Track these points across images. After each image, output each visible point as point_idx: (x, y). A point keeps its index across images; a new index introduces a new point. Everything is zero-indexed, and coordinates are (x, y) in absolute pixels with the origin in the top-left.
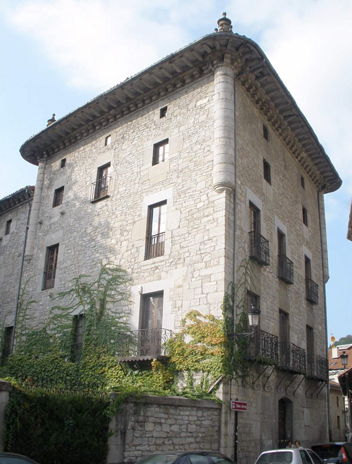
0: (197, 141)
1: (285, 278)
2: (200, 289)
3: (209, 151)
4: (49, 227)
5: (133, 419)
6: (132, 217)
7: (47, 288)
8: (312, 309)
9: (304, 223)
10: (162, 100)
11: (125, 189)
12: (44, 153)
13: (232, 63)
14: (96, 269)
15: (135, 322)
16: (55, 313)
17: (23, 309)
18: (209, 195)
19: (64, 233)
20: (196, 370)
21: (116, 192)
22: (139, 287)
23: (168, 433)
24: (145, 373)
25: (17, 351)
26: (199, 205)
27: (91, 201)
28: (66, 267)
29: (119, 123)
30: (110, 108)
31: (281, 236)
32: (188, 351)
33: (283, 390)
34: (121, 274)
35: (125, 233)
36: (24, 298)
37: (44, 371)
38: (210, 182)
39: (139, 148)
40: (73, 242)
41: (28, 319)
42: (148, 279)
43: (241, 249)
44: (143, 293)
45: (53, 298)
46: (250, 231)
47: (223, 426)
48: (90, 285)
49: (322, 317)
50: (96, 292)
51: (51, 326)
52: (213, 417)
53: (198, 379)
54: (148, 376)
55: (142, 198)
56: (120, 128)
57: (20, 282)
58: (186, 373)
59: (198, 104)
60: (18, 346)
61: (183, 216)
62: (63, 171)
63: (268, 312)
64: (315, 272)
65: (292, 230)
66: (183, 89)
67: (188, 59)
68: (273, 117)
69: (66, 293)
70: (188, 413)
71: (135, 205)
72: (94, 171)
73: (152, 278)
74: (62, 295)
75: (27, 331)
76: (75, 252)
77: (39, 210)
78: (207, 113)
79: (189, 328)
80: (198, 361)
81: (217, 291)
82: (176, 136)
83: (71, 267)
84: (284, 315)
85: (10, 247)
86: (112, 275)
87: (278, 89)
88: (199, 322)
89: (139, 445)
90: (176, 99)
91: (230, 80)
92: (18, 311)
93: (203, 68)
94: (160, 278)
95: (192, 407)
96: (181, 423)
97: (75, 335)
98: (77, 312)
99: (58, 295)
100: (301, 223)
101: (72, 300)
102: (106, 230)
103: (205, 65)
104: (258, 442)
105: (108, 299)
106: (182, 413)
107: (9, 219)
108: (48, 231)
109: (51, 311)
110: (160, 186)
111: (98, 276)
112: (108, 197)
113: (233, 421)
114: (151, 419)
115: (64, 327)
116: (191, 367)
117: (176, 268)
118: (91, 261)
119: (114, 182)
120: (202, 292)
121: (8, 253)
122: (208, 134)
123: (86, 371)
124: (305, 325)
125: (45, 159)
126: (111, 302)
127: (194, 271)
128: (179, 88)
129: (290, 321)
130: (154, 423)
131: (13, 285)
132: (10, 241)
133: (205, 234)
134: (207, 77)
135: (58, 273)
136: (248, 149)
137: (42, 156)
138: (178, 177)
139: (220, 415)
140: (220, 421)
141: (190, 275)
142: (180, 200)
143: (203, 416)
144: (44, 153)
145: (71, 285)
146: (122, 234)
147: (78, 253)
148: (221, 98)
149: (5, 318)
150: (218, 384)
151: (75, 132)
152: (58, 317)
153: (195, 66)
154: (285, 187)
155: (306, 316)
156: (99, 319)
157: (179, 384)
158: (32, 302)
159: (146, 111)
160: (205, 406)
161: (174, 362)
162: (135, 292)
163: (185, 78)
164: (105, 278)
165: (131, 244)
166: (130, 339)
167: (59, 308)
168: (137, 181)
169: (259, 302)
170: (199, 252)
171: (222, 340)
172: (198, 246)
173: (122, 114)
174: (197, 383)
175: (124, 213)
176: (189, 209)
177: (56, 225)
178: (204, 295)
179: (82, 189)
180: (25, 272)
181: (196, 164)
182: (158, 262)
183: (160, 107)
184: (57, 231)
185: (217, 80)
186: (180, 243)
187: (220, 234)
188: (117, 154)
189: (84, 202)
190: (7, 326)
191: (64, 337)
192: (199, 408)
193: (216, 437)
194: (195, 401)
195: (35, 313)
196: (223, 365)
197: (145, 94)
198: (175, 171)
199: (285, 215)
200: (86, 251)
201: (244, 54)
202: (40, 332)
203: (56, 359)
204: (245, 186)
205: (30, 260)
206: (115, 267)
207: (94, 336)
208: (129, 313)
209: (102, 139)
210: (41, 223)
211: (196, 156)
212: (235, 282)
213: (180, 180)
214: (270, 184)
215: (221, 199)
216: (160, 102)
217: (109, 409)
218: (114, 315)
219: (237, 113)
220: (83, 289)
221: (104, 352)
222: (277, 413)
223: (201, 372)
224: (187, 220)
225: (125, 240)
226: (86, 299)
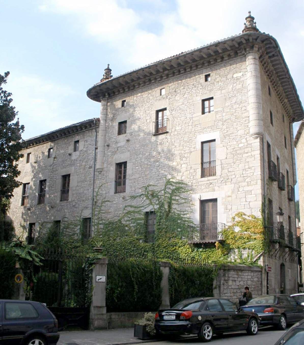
0: (236, 102)
2: (244, 199)
3: (245, 110)
4: (116, 149)
5: (223, 279)
6: (188, 149)
7: (117, 192)
10: (205, 69)
11: (180, 128)
12: (106, 94)
13: (258, 50)
14: (162, 181)
15: (197, 217)
16: (128, 210)
17: (98, 206)
18: (247, 139)
19: (130, 154)
20: (244, 248)
21: (173, 130)
22: (199, 195)
23: (238, 286)
24: (208, 250)
25: (96, 235)
26: (241, 145)
27: (153, 134)
28: (135, 179)
29: (171, 80)
30: (165, 69)
32: (238, 237)
34: (182, 186)
35: (184, 159)
36: (98, 198)
37: (124, 249)
38: (247, 131)
39: (190, 101)
40: (139, 161)
41: (104, 213)
42: (205, 190)
44: (201, 199)
45: (126, 199)
46: (165, 112)
47: (263, 280)
48: (157, 192)
50: (163, 197)
51: (126, 219)
53: (245, 254)
54: (210, 252)
55: (195, 136)
56: (172, 84)
57: (94, 186)
58: (236, 250)
59: (235, 76)
60: (96, 231)
61: (229, 151)
62: (124, 110)
66: (222, 63)
67: (228, 45)
68: (274, 80)
69: (137, 196)
70: (247, 274)
72: (153, 112)
73: (208, 190)
74: (133, 197)
75: (103, 221)
76: (142, 169)
77: (105, 136)
78: (242, 83)
79: (238, 223)
80: (245, 243)
81: (256, 201)
82: (219, 96)
83: (140, 179)
85: (80, 160)
86: (176, 186)
87: (281, 64)
88: (245, 219)
89: (226, 293)
90: (217, 70)
91: (258, 62)
92: (94, 208)
93: (238, 52)
94: (214, 190)
95: (249, 270)
97: (146, 225)
98: (148, 210)
99: (130, 198)
101: (143, 202)
102: (170, 155)
103: (240, 50)
105: (173, 202)
106: (244, 274)
107: (76, 140)
108: (116, 152)
109: (124, 208)
110: (209, 130)
111: (164, 186)
112: (167, 132)
113: (266, 278)
114: (231, 279)
115: (136, 219)
116: (241, 246)
117: (226, 185)
118: (157, 176)
119: (171, 122)
120: (246, 200)
121: (78, 165)
122: (244, 98)
123: (160, 249)
125: (106, 99)
126: (176, 204)
127: (239, 187)
128: (218, 62)
131: (86, 189)
132: (80, 156)
134: (240, 58)
137: (104, 96)
138: (223, 125)
139: (261, 275)
140: (261, 278)
141: (236, 190)
142: (226, 140)
143: (254, 276)
145: (140, 191)
147: (144, 169)
148: (253, 75)
149: (82, 212)
150: (260, 257)
151: (134, 83)
152: (131, 213)
153: (232, 50)
156: (167, 215)
157: (232, 257)
158: (106, 201)
159: (192, 75)
160: (255, 270)
161: (229, 244)
162: (196, 198)
163: (224, 56)
164: (170, 188)
165: (190, 166)
166: (193, 229)
167: (131, 206)
170: (242, 176)
171: (262, 230)
172: (241, 171)
173: (174, 74)
174: (245, 255)
175: (181, 145)
176: (233, 147)
177: (123, 148)
180: (97, 180)
181: (237, 118)
182: (211, 180)
183: (204, 73)
185: (249, 62)
186: (228, 169)
187: (257, 165)
188: (172, 102)
189: (149, 134)
190: (84, 217)
191: (138, 227)
192: (252, 271)
194: (250, 267)
196: (263, 245)
197: (193, 63)
198: (221, 120)
200: (152, 169)
201: (266, 44)
202: (116, 222)
203: (134, 241)
205: (101, 171)
206: (177, 181)
207: (164, 226)
208: (191, 212)
209: (157, 90)
211: (236, 112)
212: (265, 195)
213: (224, 127)
215: (257, 143)
216: (204, 70)
217: (213, 274)
218: (179, 212)
220: (152, 195)
221: (173, 237)
223: (248, 249)
224: (232, 154)
226: (155, 201)
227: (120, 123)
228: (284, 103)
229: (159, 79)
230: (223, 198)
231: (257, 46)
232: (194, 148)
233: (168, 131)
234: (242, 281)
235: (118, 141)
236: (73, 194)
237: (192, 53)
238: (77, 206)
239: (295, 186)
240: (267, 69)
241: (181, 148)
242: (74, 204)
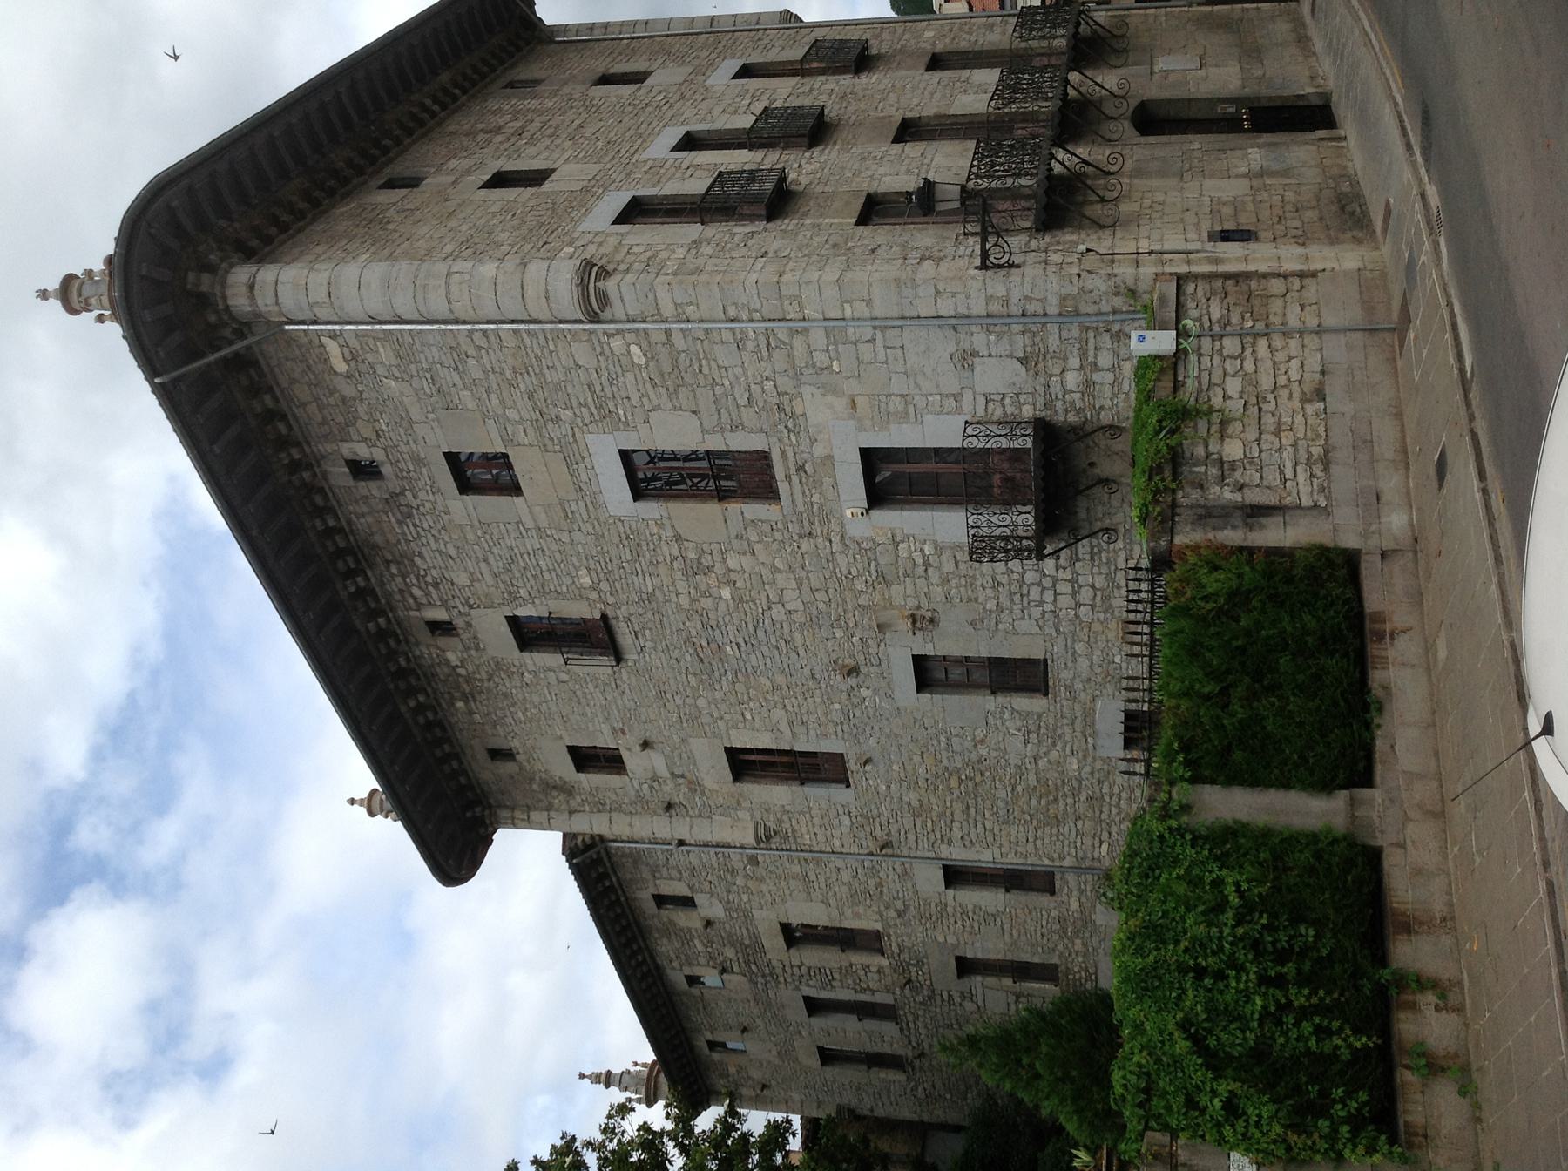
0: (457, 369)
1: (816, 130)
4: (681, 781)
5: (1215, 490)
8: (879, 57)
9: (642, 81)
13: (211, 269)
21: (594, 595)
28: (791, 723)
31: (690, 142)
33: (1112, 125)
39: (470, 536)
42: (830, 493)
43: (750, 243)
47: (1222, 268)
49: (900, 31)
52: (1200, 294)
59: (341, 367)
63: (908, 171)
64: (776, 50)
65: (669, 114)
72: (529, 662)
73: (827, 481)
82: (438, 430)
84: (908, 131)
89: (1282, 472)
96: (1221, 372)
100: (643, 91)
104: (1255, 183)
121: (745, 898)
124: (928, 75)
129: (924, 114)
130: (1222, 438)
133: (718, 339)
135: (804, 744)
136: (464, 228)
139: (1195, 277)
144: (469, 814)
154: (548, 132)
155: (903, 73)
163: (259, 409)
165: (735, 543)
168: (565, 537)
169: (884, 194)
176: (648, 385)
178: (879, 335)
179: (579, 693)
184: (691, 757)
193: (1253, 284)
195: (909, 804)
199: (631, 132)
204: (576, 235)
210: (669, 806)
213: (566, 415)
214: (553, 170)
216: (333, 482)
222: (1174, 138)
224: (676, 392)
225: (725, 559)
228: (456, 86)
229: (392, 642)
230: (861, 428)
231: (191, 276)
232: (661, 526)
233: (598, 616)
234: (1222, 385)
235: (650, 775)
236: (857, 915)
238: (899, 905)
239: (807, 18)
240: (302, 205)
241: (662, 569)
242: (895, 915)
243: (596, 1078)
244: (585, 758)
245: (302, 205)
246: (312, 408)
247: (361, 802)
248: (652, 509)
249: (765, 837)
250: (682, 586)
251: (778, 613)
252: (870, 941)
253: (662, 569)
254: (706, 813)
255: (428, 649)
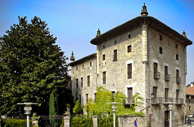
13: (146, 24)
71: (124, 64)
138: (134, 57)
146: (122, 71)
210: (100, 65)
219: (149, 38)
227: (103, 55)
237: (124, 25)
243: (73, 53)
244: (104, 56)
245: (156, 29)
246: (135, 32)
247: (99, 30)
248: (127, 66)
249: (98, 75)
250: (120, 68)
251: (118, 78)
252: (89, 85)
253: (121, 66)
254: (99, 69)
255: (113, 40)
